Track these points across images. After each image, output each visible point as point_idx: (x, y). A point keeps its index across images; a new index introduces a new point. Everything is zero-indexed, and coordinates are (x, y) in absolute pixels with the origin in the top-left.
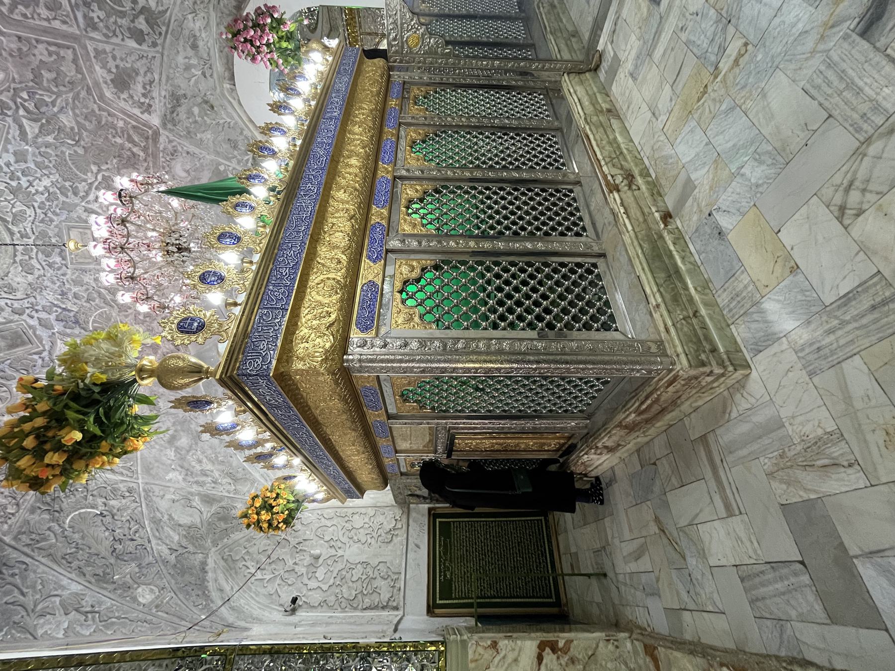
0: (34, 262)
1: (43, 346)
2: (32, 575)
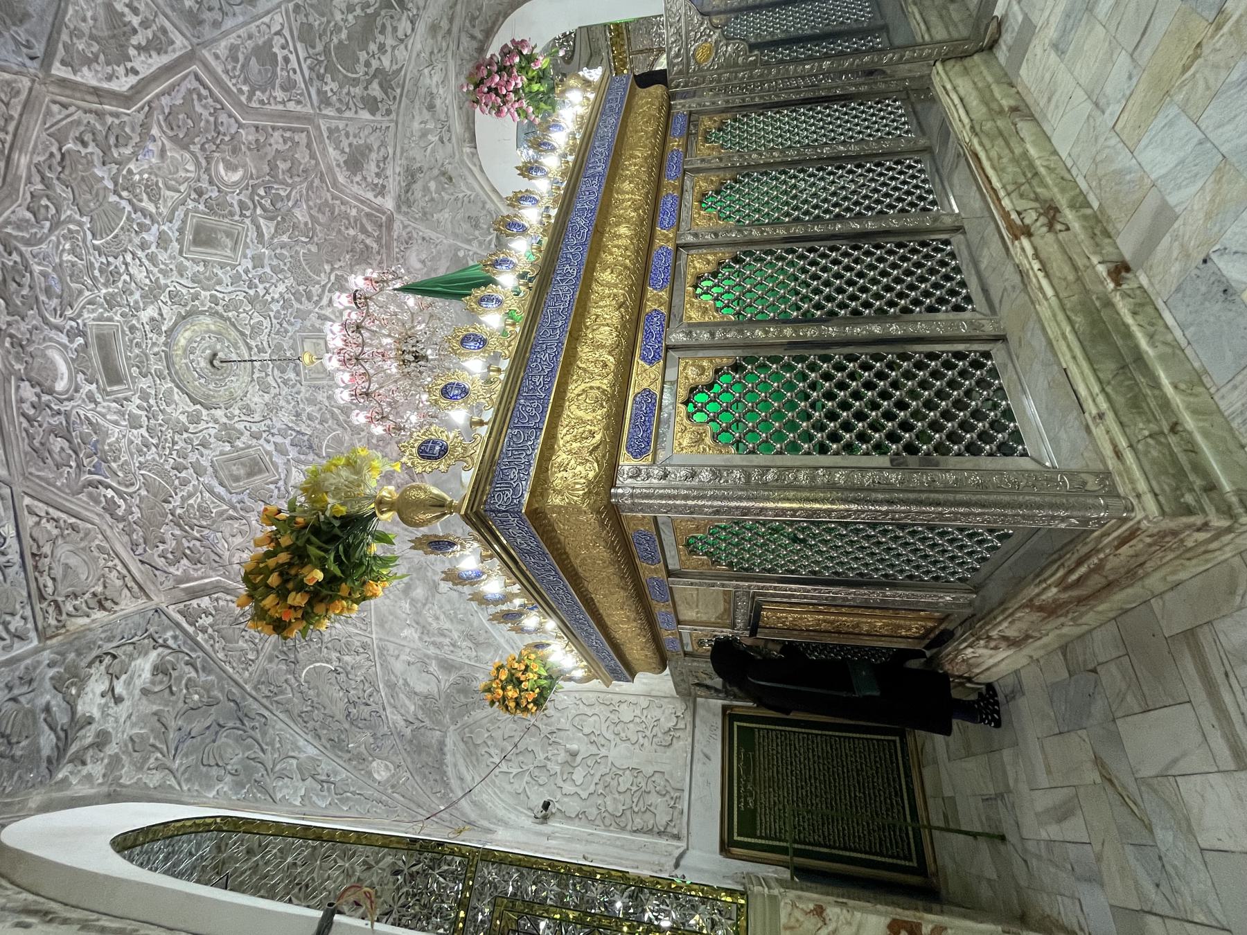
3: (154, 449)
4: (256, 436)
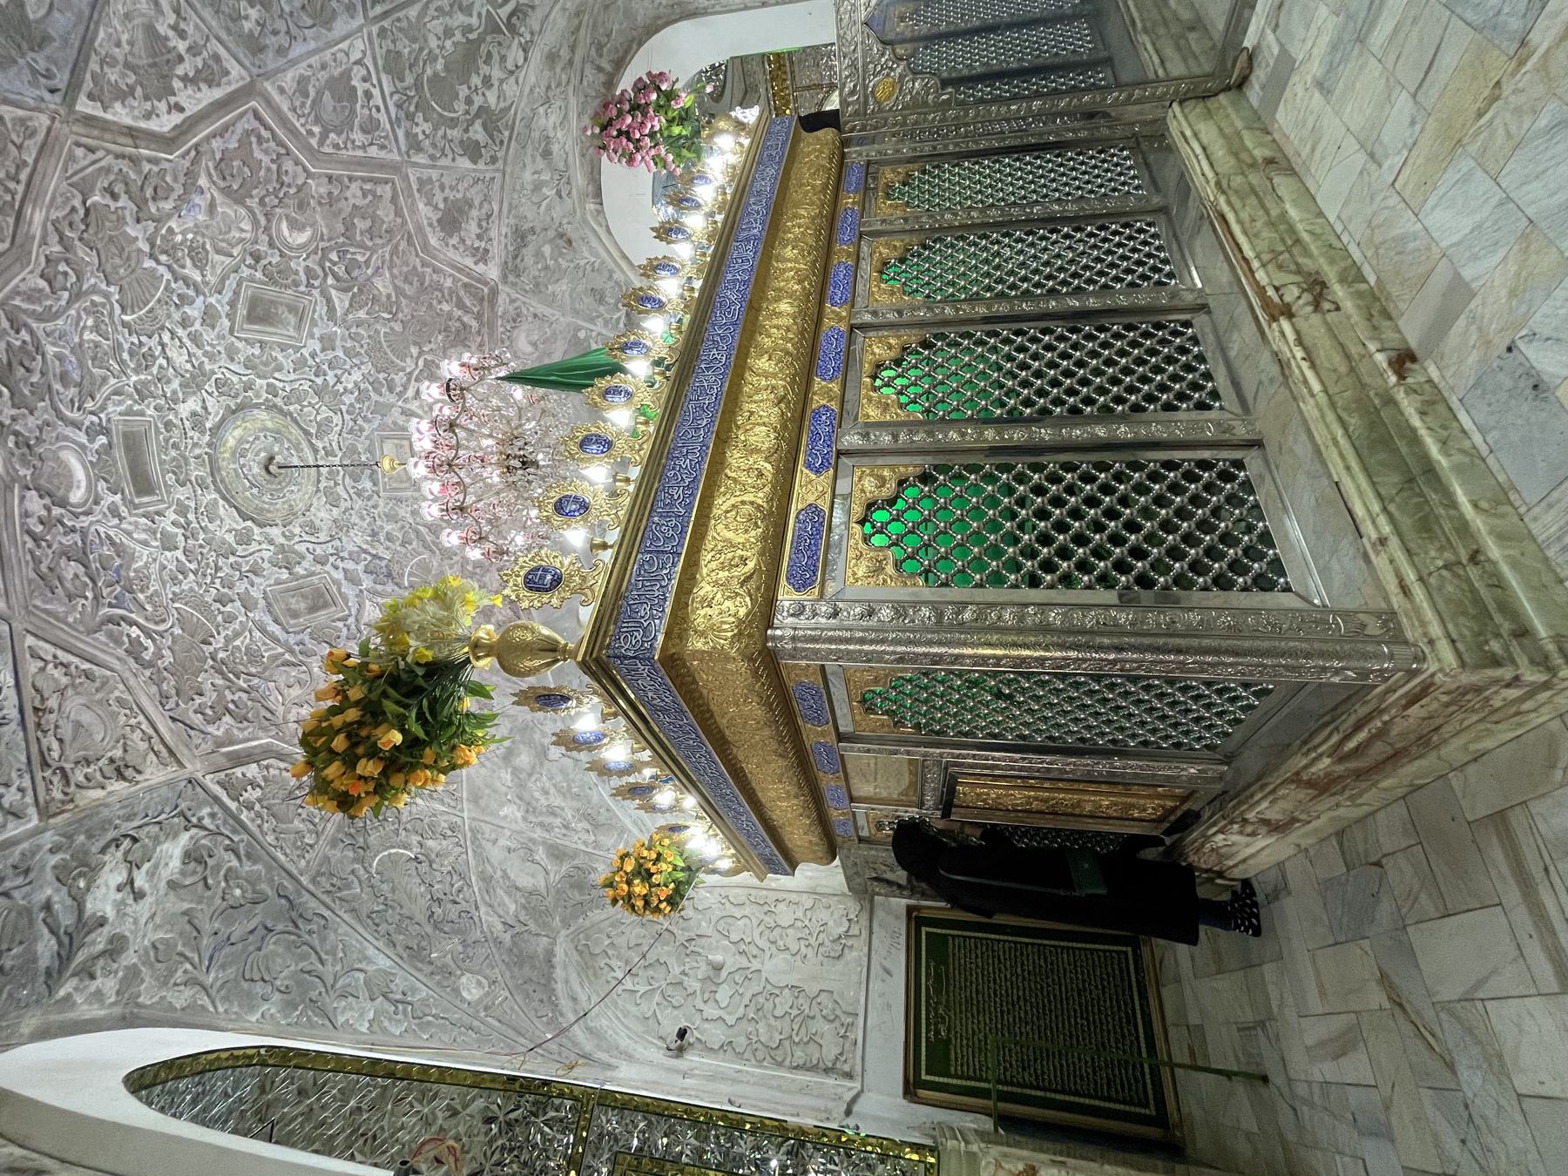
0: (340, 489)
4: (321, 561)
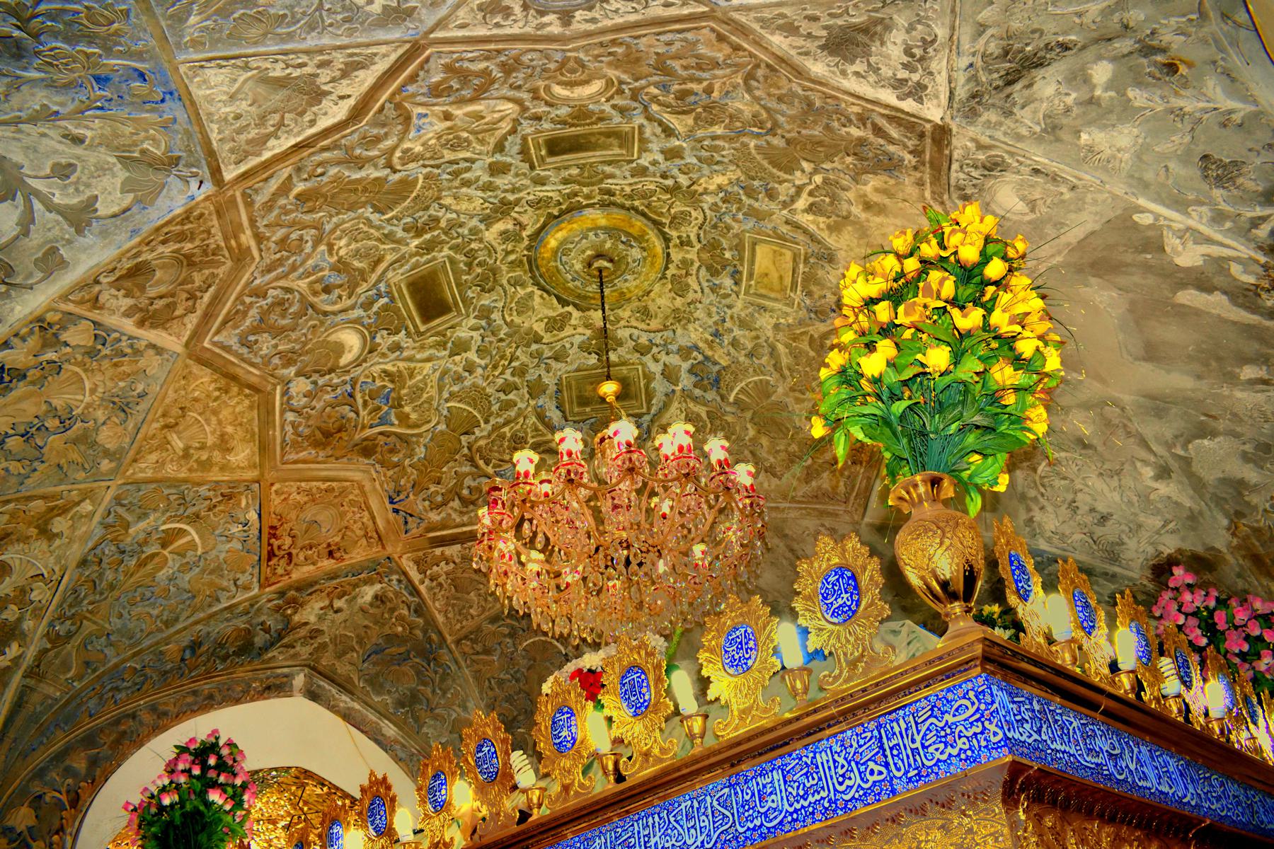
0: (692, 281)
1: (649, 409)
2: (450, 682)
3: (480, 371)
4: (642, 350)
